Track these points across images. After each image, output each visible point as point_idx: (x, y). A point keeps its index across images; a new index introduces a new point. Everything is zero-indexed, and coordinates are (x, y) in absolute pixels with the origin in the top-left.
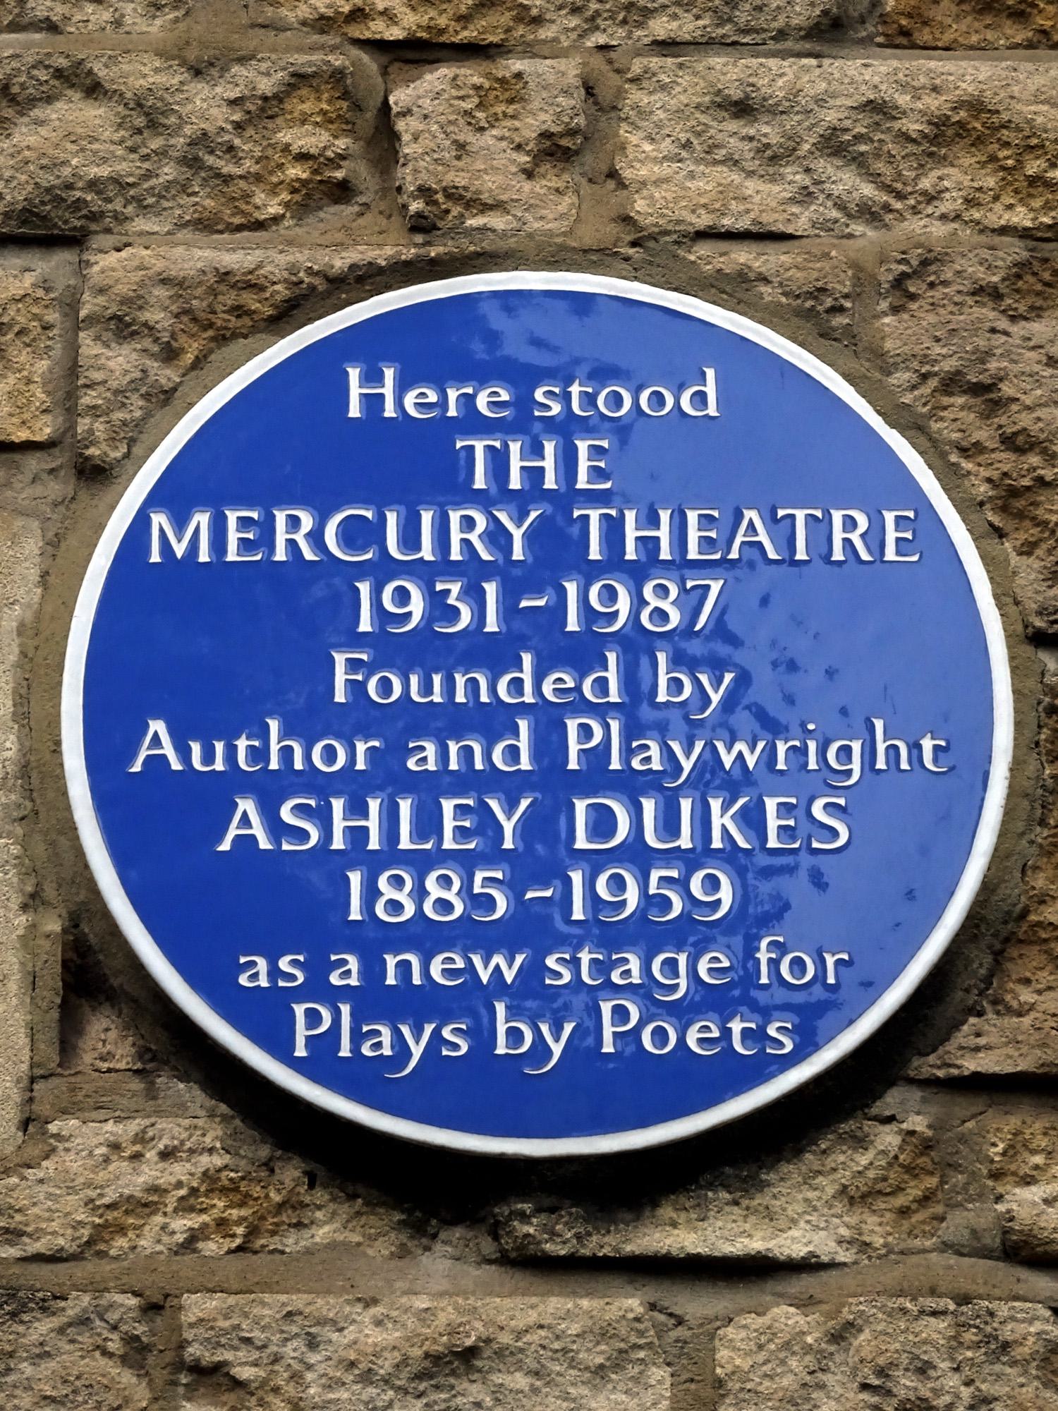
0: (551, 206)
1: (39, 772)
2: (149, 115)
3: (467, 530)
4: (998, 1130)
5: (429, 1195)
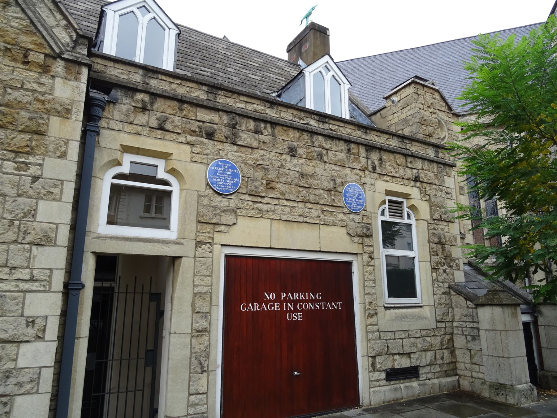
0: (225, 157)
1: (206, 176)
2: (211, 151)
3: (222, 169)
4: (240, 194)
5: (220, 194)
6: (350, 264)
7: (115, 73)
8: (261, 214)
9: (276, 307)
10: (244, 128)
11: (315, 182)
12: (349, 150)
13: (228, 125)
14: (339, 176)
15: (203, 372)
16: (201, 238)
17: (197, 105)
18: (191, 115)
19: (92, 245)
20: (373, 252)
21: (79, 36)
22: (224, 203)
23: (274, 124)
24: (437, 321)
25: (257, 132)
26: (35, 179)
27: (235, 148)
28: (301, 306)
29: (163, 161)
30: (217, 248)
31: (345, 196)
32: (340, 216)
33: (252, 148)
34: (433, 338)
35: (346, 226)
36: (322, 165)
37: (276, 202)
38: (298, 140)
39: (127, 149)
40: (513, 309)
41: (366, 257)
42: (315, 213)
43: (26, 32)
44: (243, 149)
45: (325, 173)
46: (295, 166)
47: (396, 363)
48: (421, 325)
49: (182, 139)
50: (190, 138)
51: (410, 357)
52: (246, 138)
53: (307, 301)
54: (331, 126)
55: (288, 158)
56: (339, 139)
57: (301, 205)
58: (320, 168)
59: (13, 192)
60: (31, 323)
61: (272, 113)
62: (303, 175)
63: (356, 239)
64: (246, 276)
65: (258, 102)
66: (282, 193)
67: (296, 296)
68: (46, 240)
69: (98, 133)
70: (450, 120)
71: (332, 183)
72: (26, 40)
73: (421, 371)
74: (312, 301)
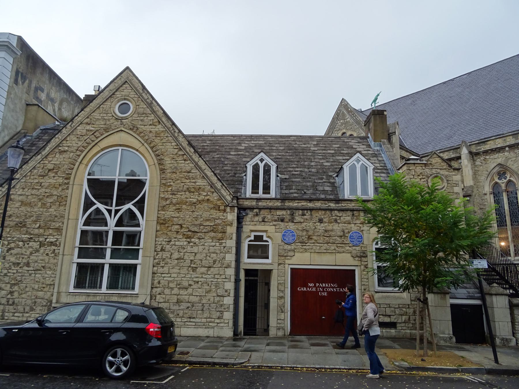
6: (354, 270)
7: (247, 203)
8: (306, 250)
9: (314, 289)
10: (297, 214)
11: (333, 233)
12: (353, 215)
13: (290, 215)
14: (347, 229)
15: (282, 312)
16: (280, 262)
17: (277, 209)
18: (275, 214)
19: (243, 267)
20: (367, 265)
21: (233, 197)
22: (289, 247)
23: (311, 210)
24: (411, 301)
25: (303, 215)
26: (224, 247)
27: (293, 224)
28: (326, 290)
29: (265, 233)
30: (286, 266)
31: (350, 238)
32: (348, 248)
33: (301, 223)
34: (407, 309)
35: (351, 253)
36: (337, 225)
37: (313, 244)
38: (325, 214)
39: (252, 231)
40: (442, 295)
41: (362, 267)
42: (333, 248)
43: (218, 200)
44: (297, 224)
45: (339, 228)
46: (322, 227)
47: (380, 319)
48: (400, 301)
49: (271, 224)
50: (274, 223)
51: (390, 317)
52: (298, 219)
53: (330, 288)
54: (343, 205)
55: (319, 224)
56: (347, 210)
57: (325, 245)
58: (336, 227)
59: (219, 252)
60: (226, 291)
61: (310, 205)
62: (326, 231)
63: (357, 259)
64: (299, 276)
65: (304, 201)
66: (316, 241)
67: (324, 285)
68: (228, 266)
69: (242, 227)
70: (451, 174)
71: (342, 233)
72: (219, 203)
73: (398, 325)
74: (332, 287)
